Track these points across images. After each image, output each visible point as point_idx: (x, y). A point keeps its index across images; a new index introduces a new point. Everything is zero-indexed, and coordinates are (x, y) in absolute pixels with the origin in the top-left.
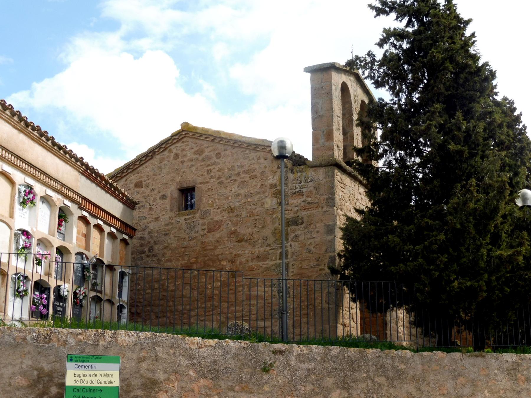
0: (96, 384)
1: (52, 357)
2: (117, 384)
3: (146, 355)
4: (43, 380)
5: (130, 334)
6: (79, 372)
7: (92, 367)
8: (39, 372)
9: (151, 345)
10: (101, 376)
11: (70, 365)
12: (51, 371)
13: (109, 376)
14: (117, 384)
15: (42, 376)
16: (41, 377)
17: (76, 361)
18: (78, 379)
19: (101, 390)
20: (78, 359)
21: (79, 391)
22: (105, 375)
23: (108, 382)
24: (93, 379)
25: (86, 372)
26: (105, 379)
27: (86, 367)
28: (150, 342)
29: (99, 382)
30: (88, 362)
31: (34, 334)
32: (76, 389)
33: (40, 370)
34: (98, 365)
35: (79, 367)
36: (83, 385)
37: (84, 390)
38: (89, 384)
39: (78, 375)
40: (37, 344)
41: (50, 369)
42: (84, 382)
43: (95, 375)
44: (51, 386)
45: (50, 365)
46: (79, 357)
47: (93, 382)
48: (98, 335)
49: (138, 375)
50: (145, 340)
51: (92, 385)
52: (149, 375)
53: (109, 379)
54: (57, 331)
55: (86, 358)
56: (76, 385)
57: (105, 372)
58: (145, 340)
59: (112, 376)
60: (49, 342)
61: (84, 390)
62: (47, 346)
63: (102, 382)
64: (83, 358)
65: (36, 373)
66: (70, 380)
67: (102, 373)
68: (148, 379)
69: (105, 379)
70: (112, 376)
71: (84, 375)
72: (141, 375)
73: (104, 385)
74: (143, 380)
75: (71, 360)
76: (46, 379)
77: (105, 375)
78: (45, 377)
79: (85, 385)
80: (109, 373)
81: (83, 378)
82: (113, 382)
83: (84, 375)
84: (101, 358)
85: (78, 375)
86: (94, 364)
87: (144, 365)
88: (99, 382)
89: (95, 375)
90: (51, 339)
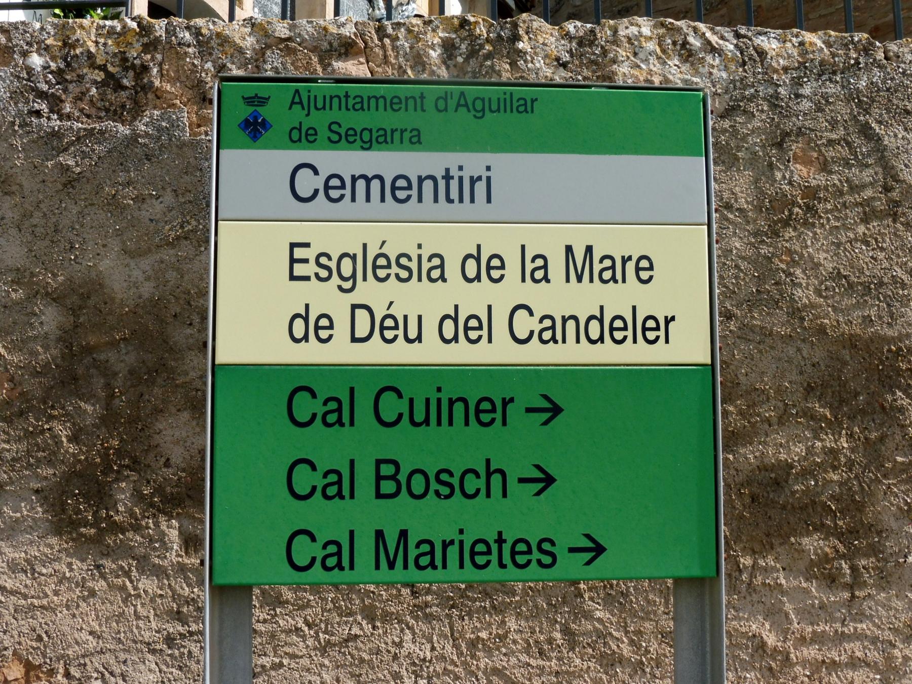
0: (499, 351)
1: (156, 208)
2: (690, 345)
3: (818, 179)
4: (107, 372)
5: (695, 42)
6: (335, 235)
7: (456, 191)
8: (75, 311)
9: (843, 111)
10: (537, 270)
11: (247, 173)
12: (155, 306)
13: (612, 271)
14: (690, 345)
15: (92, 340)
16: (88, 350)
17: (302, 137)
18: (325, 298)
19: (548, 400)
20: (319, 120)
21: (338, 413)
22: (582, 265)
23: (614, 329)
24: (473, 299)
25: (400, 235)
26: (584, 298)
27: (398, 190)
28: (831, 89)
29: (524, 324)
30: (415, 140)
31: (36, 61)
32: (314, 399)
33: (82, 300)
34: (511, 168)
35: (334, 188)
36: (375, 353)
37: (391, 406)
38: (432, 352)
39: (326, 267)
40: (56, 123)
41: (147, 289)
42: (387, 327)
43: (488, 267)
44: (158, 411)
45: (146, 263)
46: (328, 102)
47: (472, 328)
48: (473, 53)
49: (781, 315)
50: (797, 82)
51: (462, 353)
52: (845, 318)
53: (618, 299)
54: (187, 36)
55: (394, 104)
56: (312, 353)
57: (579, 237)
58: (797, 82)
59: (644, 268)
60: (137, 111)
61: (391, 406)
62: (123, 130)
63: (552, 330)
64: (361, 104)
65: (50, 319)
66: (259, 304)
67: (550, 241)
68: (852, 342)
69: (584, 298)
70: (644, 268)
71: (379, 266)
72: (796, 312)
73: (572, 353)
74: (819, 355)
75: (255, 129)
76: (123, 360)
77: (582, 265)
78: (113, 344)
79: (400, 353)
80: (612, 241)
81: (369, 291)
82: (655, 328)
83: (379, 266)
84: (526, 107)
85: (326, 267)
86: (473, 163)
87: (817, 247)
88: (524, 324)
89: (488, 267)
90: (148, 88)
